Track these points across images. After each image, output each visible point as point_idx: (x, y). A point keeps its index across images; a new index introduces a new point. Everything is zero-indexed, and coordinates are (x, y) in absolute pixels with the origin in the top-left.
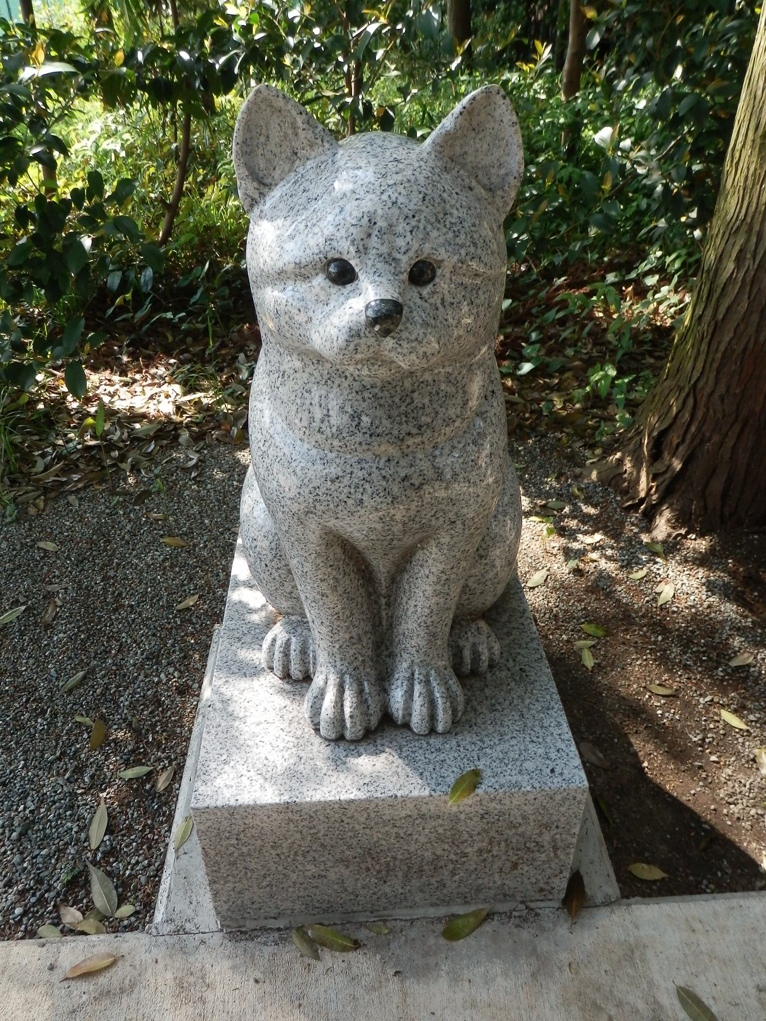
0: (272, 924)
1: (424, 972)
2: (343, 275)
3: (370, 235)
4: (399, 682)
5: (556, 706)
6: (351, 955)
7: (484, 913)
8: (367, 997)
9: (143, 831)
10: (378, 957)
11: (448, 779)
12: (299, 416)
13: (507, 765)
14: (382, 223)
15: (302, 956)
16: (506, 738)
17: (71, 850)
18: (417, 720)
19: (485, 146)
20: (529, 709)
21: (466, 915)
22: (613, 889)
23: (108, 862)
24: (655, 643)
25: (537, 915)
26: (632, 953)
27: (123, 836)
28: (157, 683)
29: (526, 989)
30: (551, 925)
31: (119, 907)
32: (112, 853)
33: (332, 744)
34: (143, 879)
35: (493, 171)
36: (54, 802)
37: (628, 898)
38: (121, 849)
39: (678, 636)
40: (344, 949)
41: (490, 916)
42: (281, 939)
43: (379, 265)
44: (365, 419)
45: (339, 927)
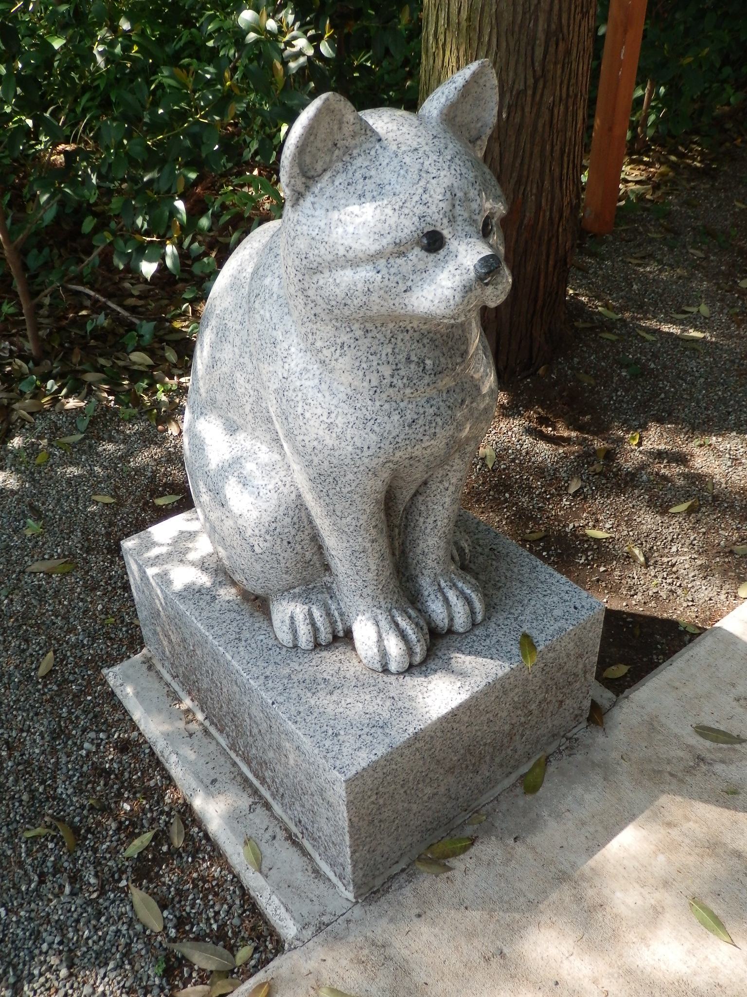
0: (396, 869)
1: (534, 825)
2: (433, 242)
3: (454, 206)
4: (433, 597)
5: (538, 563)
6: (473, 850)
7: (543, 760)
8: (509, 869)
9: (195, 886)
10: (493, 838)
11: (513, 652)
12: (367, 378)
13: (543, 620)
14: (460, 194)
15: (437, 876)
16: (526, 602)
17: (138, 946)
18: (461, 621)
19: (469, 107)
20: (522, 575)
21: (531, 770)
22: (609, 694)
23: (185, 932)
24: (506, 500)
25: (577, 740)
26: (652, 726)
27: (180, 902)
28: (87, 755)
29: (608, 790)
30: (591, 741)
31: (234, 956)
32: (181, 922)
33: (406, 674)
34: (236, 921)
35: (472, 125)
36: (77, 921)
37: (622, 692)
38: (188, 914)
39: (519, 487)
40: (465, 849)
41: (547, 760)
42: (411, 875)
43: (467, 228)
44: (428, 362)
45: (448, 838)
